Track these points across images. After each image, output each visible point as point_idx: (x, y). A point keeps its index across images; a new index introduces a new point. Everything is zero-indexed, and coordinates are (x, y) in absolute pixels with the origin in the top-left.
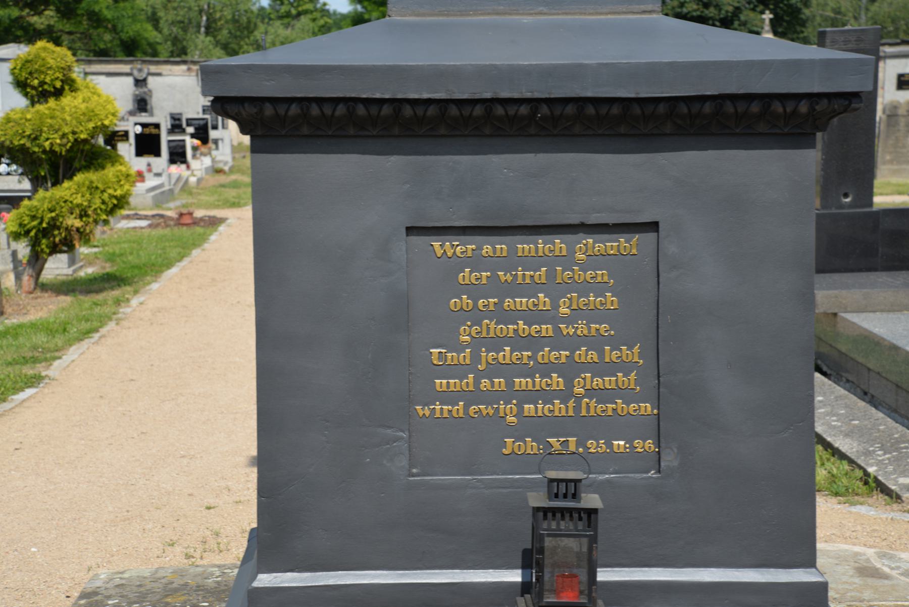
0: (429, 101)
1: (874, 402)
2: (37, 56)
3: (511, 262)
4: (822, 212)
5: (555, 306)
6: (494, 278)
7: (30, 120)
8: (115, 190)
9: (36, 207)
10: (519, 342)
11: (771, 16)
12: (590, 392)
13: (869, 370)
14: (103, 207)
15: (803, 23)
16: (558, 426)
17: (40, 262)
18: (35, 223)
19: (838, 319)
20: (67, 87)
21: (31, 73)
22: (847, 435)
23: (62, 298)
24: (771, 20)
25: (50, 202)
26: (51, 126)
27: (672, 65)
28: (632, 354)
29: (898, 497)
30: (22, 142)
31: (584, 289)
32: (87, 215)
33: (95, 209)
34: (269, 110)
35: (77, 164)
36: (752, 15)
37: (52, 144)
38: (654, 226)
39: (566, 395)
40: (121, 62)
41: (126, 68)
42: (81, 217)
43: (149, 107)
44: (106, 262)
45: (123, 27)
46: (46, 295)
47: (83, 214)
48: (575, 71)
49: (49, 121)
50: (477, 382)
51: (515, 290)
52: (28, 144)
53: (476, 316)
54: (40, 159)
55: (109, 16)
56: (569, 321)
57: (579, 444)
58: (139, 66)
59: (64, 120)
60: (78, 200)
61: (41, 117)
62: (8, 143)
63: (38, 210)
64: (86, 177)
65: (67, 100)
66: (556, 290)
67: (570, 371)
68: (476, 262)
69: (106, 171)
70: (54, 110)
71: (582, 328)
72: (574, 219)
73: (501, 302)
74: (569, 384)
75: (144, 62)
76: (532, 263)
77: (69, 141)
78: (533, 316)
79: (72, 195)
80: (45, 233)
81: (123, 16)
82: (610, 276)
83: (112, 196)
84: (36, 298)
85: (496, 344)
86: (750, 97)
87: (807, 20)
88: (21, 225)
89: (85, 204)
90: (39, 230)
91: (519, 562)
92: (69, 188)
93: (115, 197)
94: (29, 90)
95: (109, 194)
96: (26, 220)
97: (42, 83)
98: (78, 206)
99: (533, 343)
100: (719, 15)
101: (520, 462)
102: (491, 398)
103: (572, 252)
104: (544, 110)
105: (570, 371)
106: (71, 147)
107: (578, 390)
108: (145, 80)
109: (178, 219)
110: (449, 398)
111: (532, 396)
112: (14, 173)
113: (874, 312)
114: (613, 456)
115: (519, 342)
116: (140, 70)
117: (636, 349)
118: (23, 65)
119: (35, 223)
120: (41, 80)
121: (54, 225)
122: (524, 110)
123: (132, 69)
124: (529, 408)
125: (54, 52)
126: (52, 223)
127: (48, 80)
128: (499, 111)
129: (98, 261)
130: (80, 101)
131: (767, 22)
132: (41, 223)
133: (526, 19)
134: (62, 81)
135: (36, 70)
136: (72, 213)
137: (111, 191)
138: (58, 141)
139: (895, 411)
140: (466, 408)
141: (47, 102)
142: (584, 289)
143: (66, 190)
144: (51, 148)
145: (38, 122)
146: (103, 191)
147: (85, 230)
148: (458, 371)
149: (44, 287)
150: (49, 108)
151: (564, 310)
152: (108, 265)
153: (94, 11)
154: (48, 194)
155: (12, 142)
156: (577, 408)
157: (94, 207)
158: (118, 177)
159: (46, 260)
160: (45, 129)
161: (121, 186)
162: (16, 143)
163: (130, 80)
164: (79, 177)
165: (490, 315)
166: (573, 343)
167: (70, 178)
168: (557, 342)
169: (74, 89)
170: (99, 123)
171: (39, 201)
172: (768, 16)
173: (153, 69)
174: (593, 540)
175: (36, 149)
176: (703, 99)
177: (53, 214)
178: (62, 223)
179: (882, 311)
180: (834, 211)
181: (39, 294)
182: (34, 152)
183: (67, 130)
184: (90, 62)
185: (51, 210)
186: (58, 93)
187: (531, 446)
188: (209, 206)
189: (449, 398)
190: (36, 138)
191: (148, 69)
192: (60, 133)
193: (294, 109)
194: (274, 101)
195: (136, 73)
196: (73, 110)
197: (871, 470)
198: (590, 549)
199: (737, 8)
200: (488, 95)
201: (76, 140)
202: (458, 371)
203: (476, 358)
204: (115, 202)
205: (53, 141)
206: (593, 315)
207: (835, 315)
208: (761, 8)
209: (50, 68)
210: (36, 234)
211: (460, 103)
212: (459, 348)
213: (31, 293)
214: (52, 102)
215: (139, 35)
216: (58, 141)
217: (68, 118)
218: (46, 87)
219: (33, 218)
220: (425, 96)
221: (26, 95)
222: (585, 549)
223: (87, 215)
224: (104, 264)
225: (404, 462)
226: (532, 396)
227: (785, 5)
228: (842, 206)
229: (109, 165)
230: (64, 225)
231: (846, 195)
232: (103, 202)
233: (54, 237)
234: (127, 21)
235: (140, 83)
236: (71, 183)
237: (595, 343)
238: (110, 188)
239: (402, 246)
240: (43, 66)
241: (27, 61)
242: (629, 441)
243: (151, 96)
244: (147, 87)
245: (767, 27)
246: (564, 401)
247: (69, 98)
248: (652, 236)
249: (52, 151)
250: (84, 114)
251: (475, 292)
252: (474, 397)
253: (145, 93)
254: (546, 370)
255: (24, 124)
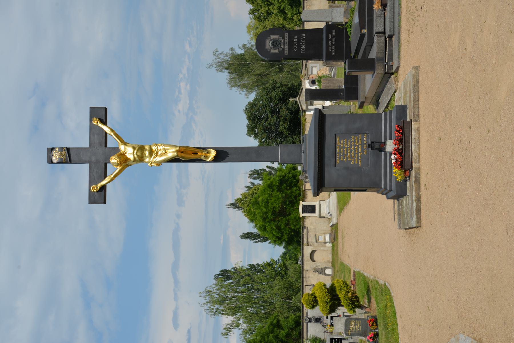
0: (318, 163)
1: (383, 90)
2: (305, 301)
3: (340, 153)
4: (344, 99)
5: (346, 147)
6: (342, 156)
7: (322, 304)
8: (341, 284)
9: (346, 305)
10: (351, 152)
11: (291, 98)
12: (358, 143)
13: (376, 91)
14: (346, 287)
15: (293, 86)
16: (362, 147)
17: (362, 306)
18: (350, 305)
19: (367, 96)
20: (314, 295)
21: (310, 303)
22: (388, 97)
23: (372, 301)
24: (292, 98)
25: (344, 300)
26: (324, 298)
27: (314, 132)
28: (353, 137)
29: (395, 90)
30: (328, 307)
31: (344, 144)
32: (348, 291)
33: (347, 289)
34: (319, 184)
35: (334, 294)
36: (290, 104)
37: (329, 299)
38: (335, 135)
39: (358, 146)
40: (303, 327)
41: (305, 325)
42: (349, 293)
43: (319, 318)
44: (364, 298)
45: (291, 326)
46: (371, 305)
47: (348, 292)
48: (315, 145)
49: (323, 299)
50: (356, 158)
51: (343, 153)
52: (329, 305)
53: (347, 158)
54: (333, 303)
55: (287, 330)
56: (348, 145)
57: (365, 144)
58: (304, 320)
59: (322, 295)
60: (344, 293)
61: (322, 301)
62: (329, 310)
63: (347, 304)
64: (338, 291)
65: (317, 295)
66: (344, 147)
67: (355, 145)
68: (340, 158)
69: (336, 286)
70: (320, 298)
71: (349, 144)
72: (334, 145)
73: (345, 154)
74: (357, 145)
75: (303, 318)
76: (340, 151)
77: (328, 294)
78: (347, 150)
79: (343, 295)
80: (353, 303)
81: (287, 325)
82: (342, 140)
83: (343, 285)
84: (372, 307)
85: (351, 155)
86: (319, 123)
87: (292, 85)
88: (351, 310)
89: (345, 291)
90: (353, 305)
91: (381, 153)
92: (341, 295)
93: (343, 284)
94: (314, 304)
95: (342, 285)
96: (350, 307)
97: (313, 301)
98: (345, 293)
99: (351, 150)
100: (289, 115)
101: (367, 152)
102: (358, 156)
103: (339, 145)
104: (320, 149)
105: (355, 145)
106: (330, 294)
107: (357, 144)
108: (309, 318)
109: (353, 285)
110: (358, 162)
111: (358, 151)
112: (307, 8)
113: (365, 89)
114: (366, 140)
115: (351, 152)
116: (306, 320)
117: (352, 137)
118: (308, 305)
119: (350, 305)
120: (312, 301)
121: (351, 300)
122: (319, 151)
123: (305, 323)
124: (360, 151)
125: (304, 297)
126: (350, 301)
127: (312, 299)
128: (320, 154)
129: (364, 300)
130: (317, 291)
131: (293, 99)
132: (350, 304)
133: (308, 152)
134: (312, 296)
135: (309, 302)
136: (348, 295)
137: (342, 285)
138: (328, 297)
139: (384, 87)
140: (359, 159)
141: (317, 300)
142: (344, 144)
143: (341, 296)
144: (330, 299)
145: (323, 302)
146: (341, 286)
147: (352, 292)
148: (355, 161)
149: (369, 305)
150: (319, 299)
151: (346, 146)
152: (365, 297)
153: (285, 335)
154: (342, 301)
155: (328, 309)
156: (360, 145)
157: (346, 289)
158: (337, 283)
159: (361, 304)
160: (325, 300)
161: (340, 282)
162: (329, 308)
163: (309, 323)
164: (338, 293)
165: (347, 156)
166: (351, 145)
167: (338, 295)
168: (351, 147)
169: (314, 293)
170: (323, 286)
171: (344, 304)
172: (291, 99)
173: (305, 315)
174: (376, 142)
175: (330, 303)
176: (319, 129)
177: (348, 300)
178: (350, 298)
179: (365, 88)
180: (344, 97)
181: (371, 307)
182: (331, 304)
183: (325, 295)
184: (303, 338)
185: (347, 300)
186: (315, 297)
187: (365, 151)
188: (350, 276)
189: (358, 162)
190: (327, 303)
191: (305, 317)
192: (326, 296)
193: (319, 181)
194: (318, 183)
195: (306, 322)
196: (320, 293)
197: (392, 94)
198: (377, 143)
199: (287, 109)
200: (318, 156)
201: (328, 293)
202: (355, 161)
203: (353, 158)
204: (345, 284)
205: (328, 298)
206: (347, 142)
207: (366, 97)
208: (287, 101)
209: (309, 298)
210: (354, 305)
211: (318, 159)
212: (351, 160)
213: (370, 309)
214: (318, 299)
215: (293, 320)
216: (328, 297)
217: (322, 294)
218: (313, 300)
219: (349, 306)
220: (317, 164)
221: (316, 306)
222: (377, 143)
223: (348, 291)
224: (365, 298)
225: (367, 168)
226: (358, 151)
227: (287, 93)
228: (343, 95)
229: (335, 285)
230: (351, 297)
231: (341, 94)
232: (345, 287)
233: (354, 300)
234: (289, 324)
235: (310, 320)
236: (339, 295)
237: (351, 142)
238: (341, 285)
239: (337, 168)
240: (308, 300)
241: (307, 304)
242: (365, 138)
243: (315, 317)
244: (312, 318)
245: (295, 99)
246: (359, 146)
247: (316, 294)
248: (337, 135)
249: (331, 299)
250: (321, 290)
251: (344, 158)
252: (358, 158)
253: (314, 319)
254: (355, 149)
255: (323, 306)
